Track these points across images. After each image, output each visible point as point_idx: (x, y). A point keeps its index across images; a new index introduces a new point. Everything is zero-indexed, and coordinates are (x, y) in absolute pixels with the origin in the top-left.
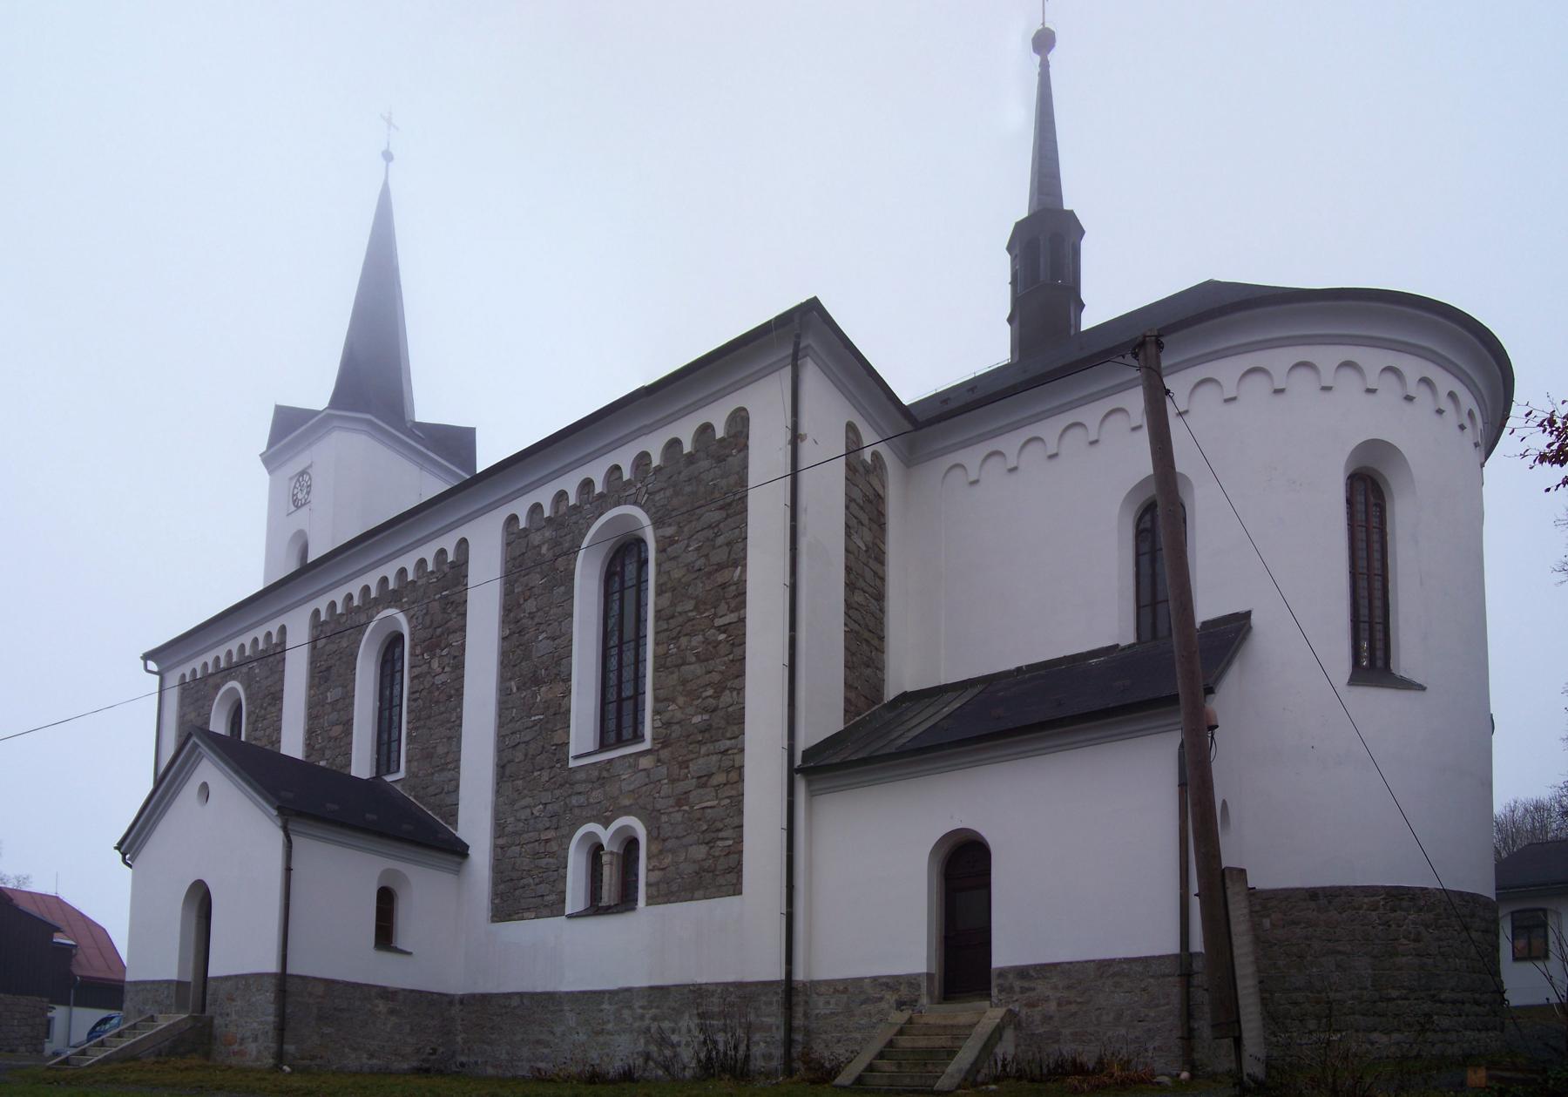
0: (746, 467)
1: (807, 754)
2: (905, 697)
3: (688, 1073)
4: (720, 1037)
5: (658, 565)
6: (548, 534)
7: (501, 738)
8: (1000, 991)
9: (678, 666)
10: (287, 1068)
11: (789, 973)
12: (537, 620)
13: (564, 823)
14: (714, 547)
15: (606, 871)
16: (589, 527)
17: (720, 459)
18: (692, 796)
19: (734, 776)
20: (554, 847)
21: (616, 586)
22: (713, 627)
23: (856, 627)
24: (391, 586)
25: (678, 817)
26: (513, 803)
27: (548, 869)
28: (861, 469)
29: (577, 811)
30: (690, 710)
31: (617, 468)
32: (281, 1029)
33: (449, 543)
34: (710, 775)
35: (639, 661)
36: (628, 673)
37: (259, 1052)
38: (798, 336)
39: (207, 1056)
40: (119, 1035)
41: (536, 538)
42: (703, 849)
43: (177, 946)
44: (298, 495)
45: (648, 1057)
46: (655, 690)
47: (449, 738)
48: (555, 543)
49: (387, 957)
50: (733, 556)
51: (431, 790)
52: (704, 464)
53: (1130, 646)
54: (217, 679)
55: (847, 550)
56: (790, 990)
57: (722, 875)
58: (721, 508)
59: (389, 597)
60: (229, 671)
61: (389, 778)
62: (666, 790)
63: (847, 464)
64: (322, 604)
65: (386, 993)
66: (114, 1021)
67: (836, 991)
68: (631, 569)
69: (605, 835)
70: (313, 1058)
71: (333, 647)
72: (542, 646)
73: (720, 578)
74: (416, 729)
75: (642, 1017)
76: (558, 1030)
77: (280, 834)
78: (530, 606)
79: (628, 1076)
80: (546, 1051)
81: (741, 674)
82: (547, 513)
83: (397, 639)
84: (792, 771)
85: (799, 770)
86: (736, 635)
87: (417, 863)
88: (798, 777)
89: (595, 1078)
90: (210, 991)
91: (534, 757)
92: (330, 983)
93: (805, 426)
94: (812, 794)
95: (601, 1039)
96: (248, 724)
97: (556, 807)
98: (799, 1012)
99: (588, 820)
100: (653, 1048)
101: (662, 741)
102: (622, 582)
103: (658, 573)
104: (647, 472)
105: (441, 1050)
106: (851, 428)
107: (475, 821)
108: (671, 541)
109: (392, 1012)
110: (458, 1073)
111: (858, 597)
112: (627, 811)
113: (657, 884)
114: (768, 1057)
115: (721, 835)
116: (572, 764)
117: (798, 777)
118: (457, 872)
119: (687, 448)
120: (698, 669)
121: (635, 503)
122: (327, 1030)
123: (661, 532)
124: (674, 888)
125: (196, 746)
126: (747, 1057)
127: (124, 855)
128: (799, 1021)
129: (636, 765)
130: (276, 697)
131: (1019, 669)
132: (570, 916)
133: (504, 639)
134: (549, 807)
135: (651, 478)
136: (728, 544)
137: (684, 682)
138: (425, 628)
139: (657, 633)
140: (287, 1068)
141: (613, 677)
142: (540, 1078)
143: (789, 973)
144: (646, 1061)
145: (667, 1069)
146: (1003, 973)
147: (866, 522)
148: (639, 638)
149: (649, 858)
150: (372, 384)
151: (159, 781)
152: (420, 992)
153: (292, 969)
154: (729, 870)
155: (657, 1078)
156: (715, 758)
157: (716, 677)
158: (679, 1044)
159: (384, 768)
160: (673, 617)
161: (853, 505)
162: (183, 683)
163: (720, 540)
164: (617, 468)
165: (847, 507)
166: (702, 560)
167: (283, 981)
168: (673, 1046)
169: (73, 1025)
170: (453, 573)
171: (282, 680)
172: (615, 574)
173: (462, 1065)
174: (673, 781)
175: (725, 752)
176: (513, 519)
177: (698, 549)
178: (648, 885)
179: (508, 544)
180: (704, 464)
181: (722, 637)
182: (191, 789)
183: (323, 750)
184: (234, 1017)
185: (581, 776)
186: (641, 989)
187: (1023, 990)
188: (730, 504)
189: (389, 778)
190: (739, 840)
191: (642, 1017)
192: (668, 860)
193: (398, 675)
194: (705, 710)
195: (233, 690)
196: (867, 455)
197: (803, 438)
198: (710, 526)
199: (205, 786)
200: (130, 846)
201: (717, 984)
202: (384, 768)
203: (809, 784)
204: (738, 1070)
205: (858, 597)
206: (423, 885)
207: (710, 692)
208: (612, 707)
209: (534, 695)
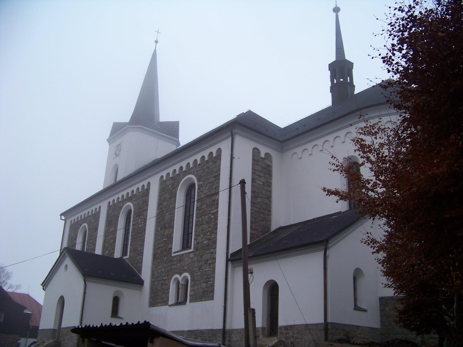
1: (232, 255)
2: (281, 228)
6: (171, 182)
8: (280, 334)
9: (201, 225)
15: (180, 290)
17: (215, 162)
18: (203, 266)
19: (214, 260)
20: (167, 282)
23: (258, 210)
25: (199, 274)
28: (261, 160)
30: (204, 239)
31: (189, 163)
33: (145, 183)
34: (208, 260)
38: (231, 131)
41: (168, 183)
42: (205, 284)
44: (116, 152)
46: (195, 232)
48: (173, 185)
52: (211, 163)
53: (346, 211)
57: (206, 294)
58: (214, 177)
59: (129, 199)
61: (124, 258)
62: (196, 265)
64: (111, 200)
67: (238, 333)
69: (180, 278)
72: (167, 216)
73: (213, 198)
77: (83, 282)
78: (165, 204)
81: (216, 229)
83: (130, 212)
84: (227, 260)
88: (229, 262)
93: (235, 155)
94: (233, 267)
98: (227, 339)
101: (196, 249)
102: (191, 196)
107: (146, 274)
116: (173, 255)
117: (229, 262)
121: (193, 174)
125: (65, 254)
127: (43, 287)
129: (189, 256)
130: (96, 229)
131: (314, 219)
137: (203, 230)
139: (197, 214)
146: (281, 327)
149: (191, 287)
150: (145, 115)
151: (61, 254)
156: (209, 255)
157: (211, 229)
160: (201, 209)
163: (214, 187)
170: (146, 192)
174: (198, 262)
175: (212, 253)
178: (190, 296)
179: (161, 184)
180: (211, 163)
181: (213, 217)
182: (63, 266)
184: (66, 341)
185: (175, 259)
186: (186, 331)
187: (286, 334)
189: (124, 258)
190: (214, 282)
197: (234, 158)
199: (66, 266)
200: (45, 284)
201: (206, 330)
203: (233, 264)
207: (209, 234)
209: (164, 232)
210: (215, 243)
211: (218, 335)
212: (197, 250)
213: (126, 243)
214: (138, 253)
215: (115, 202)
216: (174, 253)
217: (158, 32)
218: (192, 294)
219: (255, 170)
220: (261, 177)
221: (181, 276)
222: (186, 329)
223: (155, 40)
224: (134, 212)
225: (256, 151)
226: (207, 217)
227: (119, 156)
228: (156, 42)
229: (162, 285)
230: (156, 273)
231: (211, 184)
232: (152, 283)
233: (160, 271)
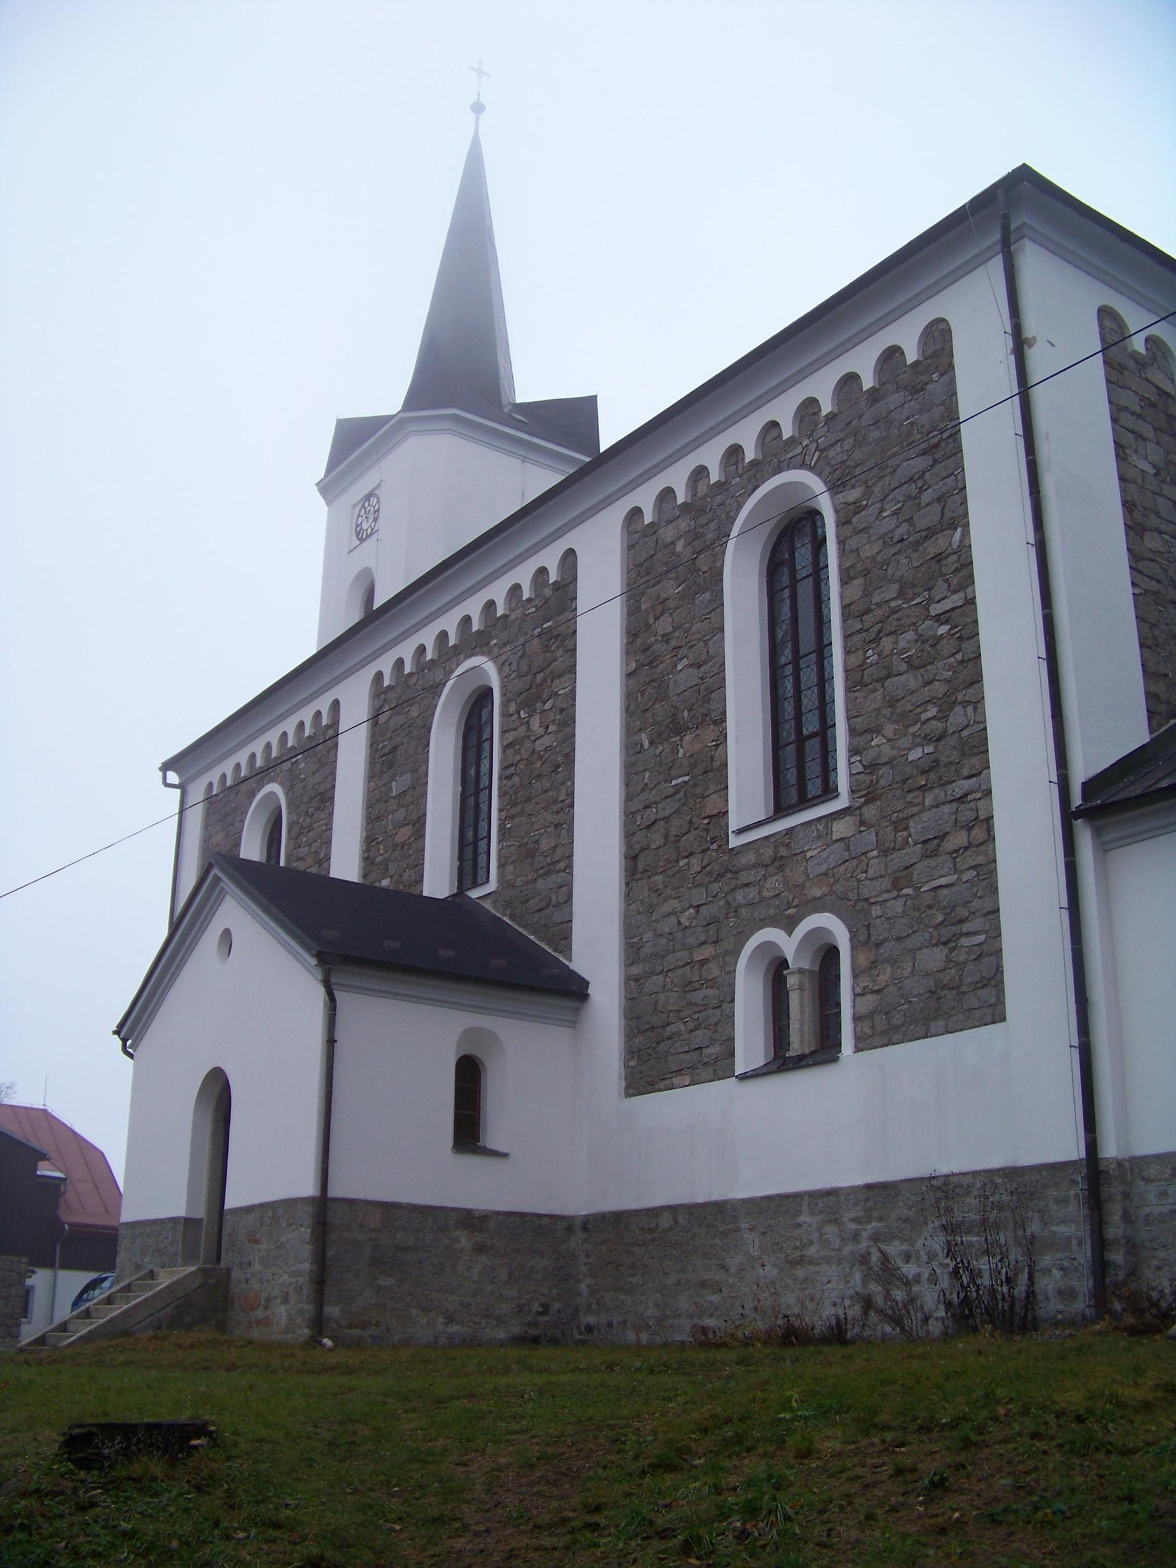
0: (955, 394)
1: (1088, 787)
3: (935, 1328)
4: (982, 1264)
5: (841, 542)
6: (683, 525)
7: (629, 816)
9: (882, 680)
10: (327, 1342)
11: (1092, 1145)
12: (673, 644)
13: (726, 934)
14: (919, 507)
15: (794, 1000)
16: (740, 507)
17: (916, 390)
19: (979, 833)
20: (714, 970)
21: (785, 579)
22: (928, 617)
23: (1154, 586)
24: (476, 626)
25: (897, 906)
26: (650, 910)
27: (705, 1007)
28: (1132, 365)
29: (744, 911)
30: (903, 742)
31: (774, 425)
32: (320, 1280)
33: (550, 558)
34: (943, 836)
35: (824, 681)
36: (809, 700)
37: (290, 1318)
39: (222, 1327)
40: (109, 1301)
41: (667, 534)
42: (940, 953)
43: (187, 1158)
45: (868, 1303)
46: (849, 719)
47: (557, 826)
48: (694, 535)
49: (471, 1163)
50: (948, 515)
51: (533, 904)
52: (895, 399)
54: (252, 783)
55: (1122, 478)
56: (1095, 1178)
57: (967, 993)
58: (925, 453)
59: (475, 641)
60: (261, 775)
62: (876, 866)
63: (1104, 362)
64: (385, 664)
65: (470, 1220)
66: (106, 1284)
68: (804, 554)
69: (788, 944)
70: (365, 1325)
71: (399, 720)
72: (683, 677)
74: (512, 818)
75: (856, 1237)
76: (734, 1262)
77: (321, 991)
78: (664, 625)
79: (838, 1335)
80: (715, 1298)
82: (681, 498)
83: (483, 696)
84: (1068, 816)
85: (1080, 813)
86: (964, 626)
87: (510, 1014)
88: (1078, 824)
89: (792, 1336)
90: (226, 1231)
91: (678, 838)
92: (388, 1208)
93: (1031, 328)
94: (1103, 848)
95: (800, 1272)
96: (289, 839)
97: (713, 909)
98: (1115, 1212)
99: (763, 923)
100: (875, 1288)
101: (866, 793)
102: (793, 572)
103: (842, 553)
104: (816, 423)
105: (556, 1306)
106: (1106, 314)
107: (596, 946)
108: (857, 507)
109: (480, 1248)
110: (583, 1342)
111: (1152, 542)
112: (818, 906)
113: (871, 1016)
114: (1068, 1294)
115: (966, 927)
116: (734, 842)
117: (1078, 824)
118: (573, 1024)
119: (868, 382)
120: (911, 680)
121: (803, 466)
122: (385, 1281)
123: (841, 498)
124: (898, 1019)
126: (1030, 1295)
127: (124, 1041)
128: (1115, 1230)
130: (326, 798)
132: (743, 1077)
133: (629, 675)
134: (703, 910)
135: (821, 431)
136: (939, 500)
137: (892, 702)
138: (520, 676)
139: (846, 637)
140: (327, 1342)
141: (788, 708)
142: (705, 1340)
143: (1092, 1145)
144: (865, 1312)
145: (898, 1321)
147: (1150, 434)
148: (822, 648)
149: (855, 976)
150: (460, 374)
151: (174, 925)
152: (522, 1215)
153: (334, 1192)
154: (983, 983)
155: (884, 1338)
156: (946, 809)
157: (939, 688)
158: (917, 1279)
159: (468, 881)
160: (868, 611)
161: (1125, 418)
162: (210, 799)
163: (927, 497)
164: (774, 425)
165: (1114, 420)
166: (905, 527)
167: (324, 1212)
168: (907, 1283)
169: (55, 1293)
170: (559, 596)
171: (333, 774)
172: (782, 563)
173: (589, 1329)
174: (885, 852)
175: (962, 799)
176: (636, 512)
177: (896, 513)
178: (856, 1018)
179: (630, 547)
180: (895, 399)
181: (943, 630)
182: (210, 939)
183: (385, 863)
184: (257, 1267)
185: (750, 858)
186: (853, 1190)
188: (937, 446)
189: (474, 894)
190: (995, 933)
191: (856, 1237)
192: (885, 975)
193: (486, 745)
194: (927, 739)
195: (272, 795)
196: (1138, 344)
197: (1031, 343)
198: (911, 480)
199: (227, 935)
200: (132, 1029)
202: (468, 881)
203: (1097, 833)
204: (1014, 1317)
205: (1152, 542)
206: (523, 1050)
207: (932, 711)
208: (790, 752)
209: (675, 750)
210: (976, 746)
211: (1052, 1192)
212: (870, 797)
213: (470, 835)
214: (547, 858)
215: (407, 670)
216: (740, 831)
217: (480, 73)
218: (863, 1010)
219: (1122, 409)
220: (1144, 439)
221: (790, 934)
222: (850, 1176)
223: (474, 100)
224: (503, 695)
225: (1107, 323)
226: (911, 635)
227: (373, 539)
228: (478, 108)
229: (688, 986)
230: (648, 936)
231: (912, 489)
232: (634, 985)
233: (667, 925)
